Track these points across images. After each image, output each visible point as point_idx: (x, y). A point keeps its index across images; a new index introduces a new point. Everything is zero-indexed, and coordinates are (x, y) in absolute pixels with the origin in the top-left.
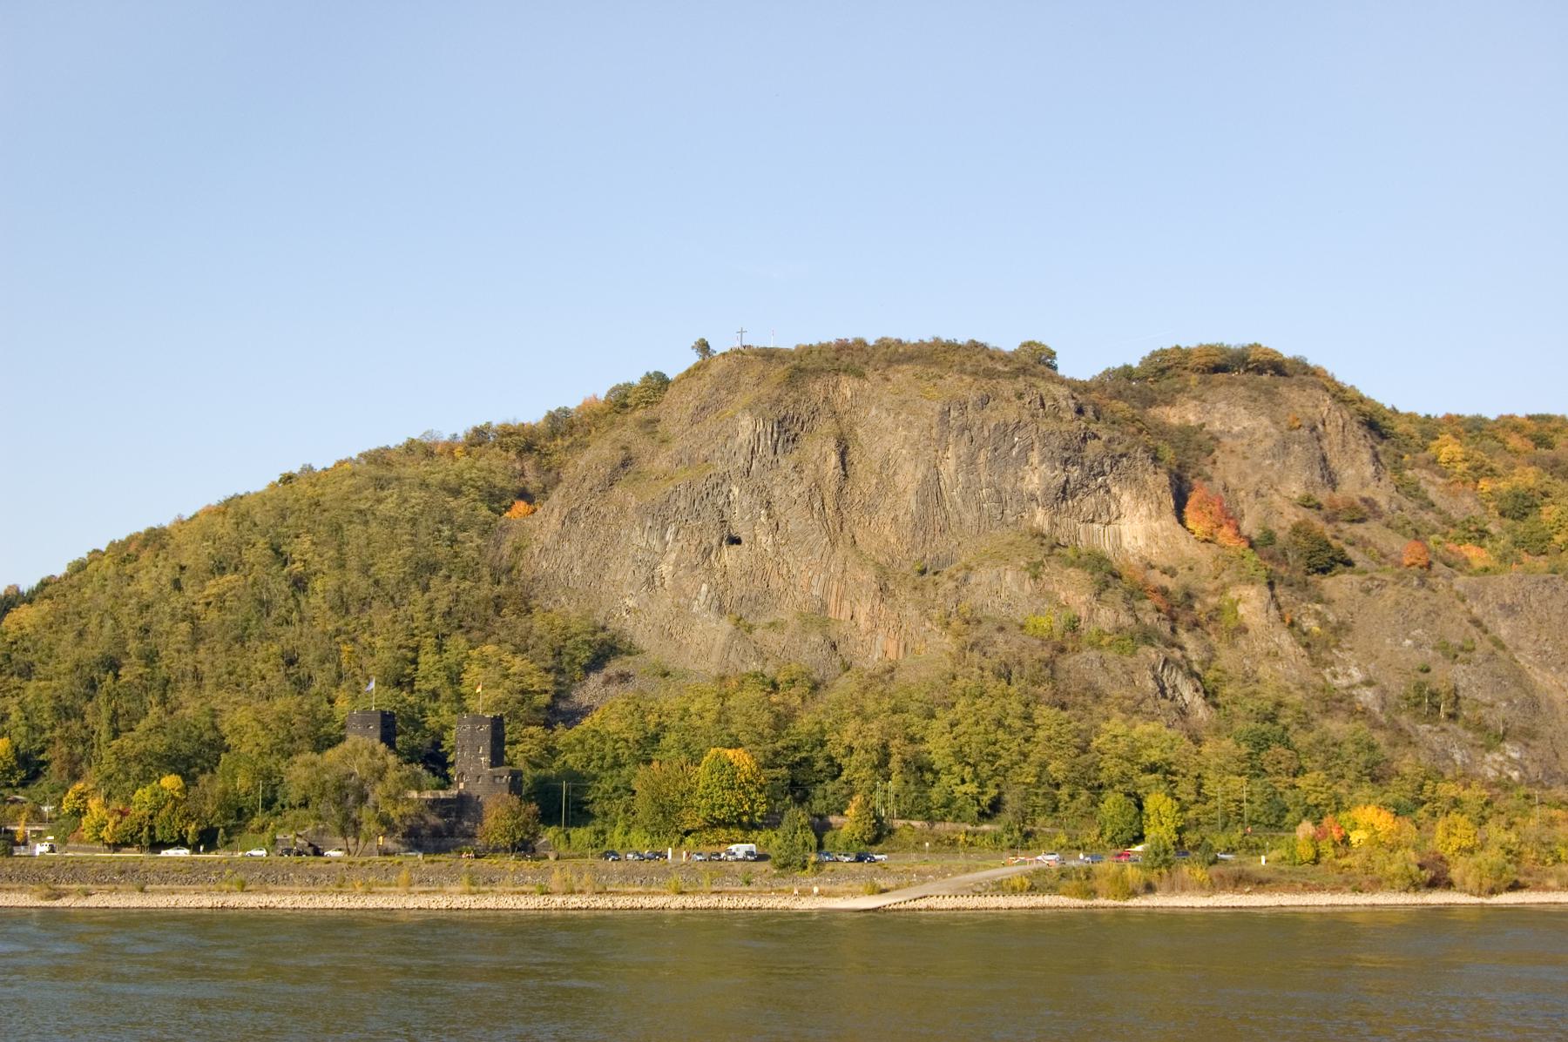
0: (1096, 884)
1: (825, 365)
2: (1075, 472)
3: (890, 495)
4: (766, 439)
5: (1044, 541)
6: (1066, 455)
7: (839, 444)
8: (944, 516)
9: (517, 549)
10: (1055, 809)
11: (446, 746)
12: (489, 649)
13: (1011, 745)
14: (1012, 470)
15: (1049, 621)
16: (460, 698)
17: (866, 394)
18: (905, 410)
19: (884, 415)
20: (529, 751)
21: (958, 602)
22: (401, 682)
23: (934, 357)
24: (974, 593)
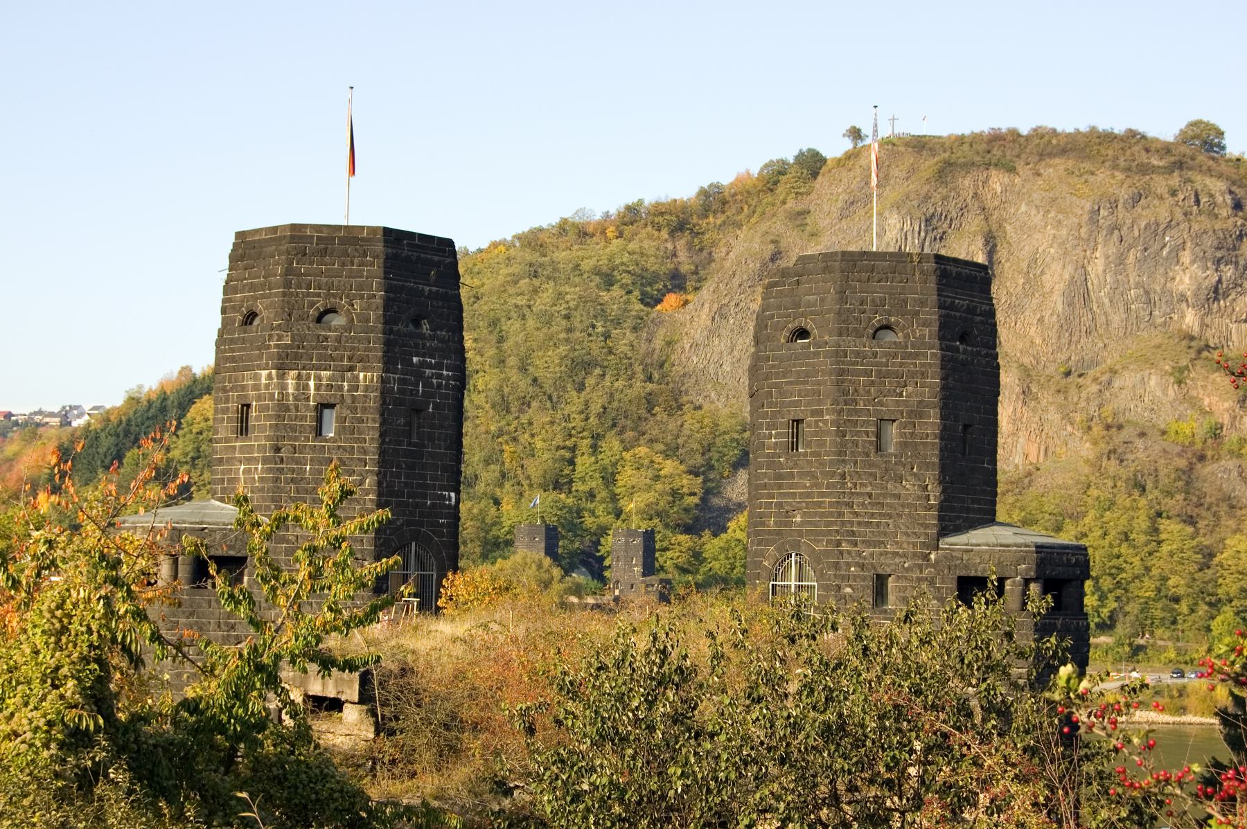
0: (1186, 702)
1: (977, 159)
2: (1229, 272)
3: (1037, 295)
4: (913, 238)
5: (1193, 344)
6: (1219, 254)
7: (987, 243)
8: (1090, 317)
9: (669, 343)
10: (1174, 622)
11: (602, 551)
12: (642, 450)
13: (1133, 560)
14: (1162, 270)
15: (1192, 427)
16: (614, 498)
17: (1017, 189)
18: (1055, 208)
19: (1034, 212)
20: (678, 558)
21: (1100, 406)
22: (558, 483)
23: (1088, 150)
24: (1117, 397)
